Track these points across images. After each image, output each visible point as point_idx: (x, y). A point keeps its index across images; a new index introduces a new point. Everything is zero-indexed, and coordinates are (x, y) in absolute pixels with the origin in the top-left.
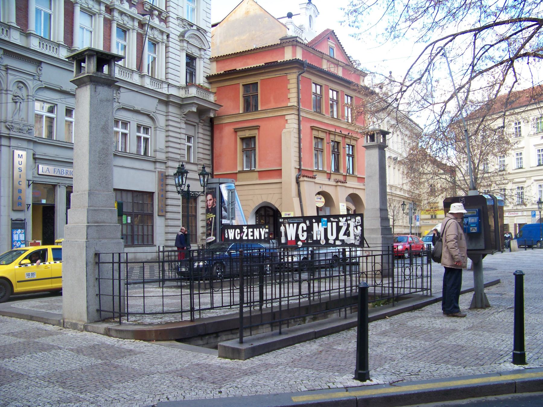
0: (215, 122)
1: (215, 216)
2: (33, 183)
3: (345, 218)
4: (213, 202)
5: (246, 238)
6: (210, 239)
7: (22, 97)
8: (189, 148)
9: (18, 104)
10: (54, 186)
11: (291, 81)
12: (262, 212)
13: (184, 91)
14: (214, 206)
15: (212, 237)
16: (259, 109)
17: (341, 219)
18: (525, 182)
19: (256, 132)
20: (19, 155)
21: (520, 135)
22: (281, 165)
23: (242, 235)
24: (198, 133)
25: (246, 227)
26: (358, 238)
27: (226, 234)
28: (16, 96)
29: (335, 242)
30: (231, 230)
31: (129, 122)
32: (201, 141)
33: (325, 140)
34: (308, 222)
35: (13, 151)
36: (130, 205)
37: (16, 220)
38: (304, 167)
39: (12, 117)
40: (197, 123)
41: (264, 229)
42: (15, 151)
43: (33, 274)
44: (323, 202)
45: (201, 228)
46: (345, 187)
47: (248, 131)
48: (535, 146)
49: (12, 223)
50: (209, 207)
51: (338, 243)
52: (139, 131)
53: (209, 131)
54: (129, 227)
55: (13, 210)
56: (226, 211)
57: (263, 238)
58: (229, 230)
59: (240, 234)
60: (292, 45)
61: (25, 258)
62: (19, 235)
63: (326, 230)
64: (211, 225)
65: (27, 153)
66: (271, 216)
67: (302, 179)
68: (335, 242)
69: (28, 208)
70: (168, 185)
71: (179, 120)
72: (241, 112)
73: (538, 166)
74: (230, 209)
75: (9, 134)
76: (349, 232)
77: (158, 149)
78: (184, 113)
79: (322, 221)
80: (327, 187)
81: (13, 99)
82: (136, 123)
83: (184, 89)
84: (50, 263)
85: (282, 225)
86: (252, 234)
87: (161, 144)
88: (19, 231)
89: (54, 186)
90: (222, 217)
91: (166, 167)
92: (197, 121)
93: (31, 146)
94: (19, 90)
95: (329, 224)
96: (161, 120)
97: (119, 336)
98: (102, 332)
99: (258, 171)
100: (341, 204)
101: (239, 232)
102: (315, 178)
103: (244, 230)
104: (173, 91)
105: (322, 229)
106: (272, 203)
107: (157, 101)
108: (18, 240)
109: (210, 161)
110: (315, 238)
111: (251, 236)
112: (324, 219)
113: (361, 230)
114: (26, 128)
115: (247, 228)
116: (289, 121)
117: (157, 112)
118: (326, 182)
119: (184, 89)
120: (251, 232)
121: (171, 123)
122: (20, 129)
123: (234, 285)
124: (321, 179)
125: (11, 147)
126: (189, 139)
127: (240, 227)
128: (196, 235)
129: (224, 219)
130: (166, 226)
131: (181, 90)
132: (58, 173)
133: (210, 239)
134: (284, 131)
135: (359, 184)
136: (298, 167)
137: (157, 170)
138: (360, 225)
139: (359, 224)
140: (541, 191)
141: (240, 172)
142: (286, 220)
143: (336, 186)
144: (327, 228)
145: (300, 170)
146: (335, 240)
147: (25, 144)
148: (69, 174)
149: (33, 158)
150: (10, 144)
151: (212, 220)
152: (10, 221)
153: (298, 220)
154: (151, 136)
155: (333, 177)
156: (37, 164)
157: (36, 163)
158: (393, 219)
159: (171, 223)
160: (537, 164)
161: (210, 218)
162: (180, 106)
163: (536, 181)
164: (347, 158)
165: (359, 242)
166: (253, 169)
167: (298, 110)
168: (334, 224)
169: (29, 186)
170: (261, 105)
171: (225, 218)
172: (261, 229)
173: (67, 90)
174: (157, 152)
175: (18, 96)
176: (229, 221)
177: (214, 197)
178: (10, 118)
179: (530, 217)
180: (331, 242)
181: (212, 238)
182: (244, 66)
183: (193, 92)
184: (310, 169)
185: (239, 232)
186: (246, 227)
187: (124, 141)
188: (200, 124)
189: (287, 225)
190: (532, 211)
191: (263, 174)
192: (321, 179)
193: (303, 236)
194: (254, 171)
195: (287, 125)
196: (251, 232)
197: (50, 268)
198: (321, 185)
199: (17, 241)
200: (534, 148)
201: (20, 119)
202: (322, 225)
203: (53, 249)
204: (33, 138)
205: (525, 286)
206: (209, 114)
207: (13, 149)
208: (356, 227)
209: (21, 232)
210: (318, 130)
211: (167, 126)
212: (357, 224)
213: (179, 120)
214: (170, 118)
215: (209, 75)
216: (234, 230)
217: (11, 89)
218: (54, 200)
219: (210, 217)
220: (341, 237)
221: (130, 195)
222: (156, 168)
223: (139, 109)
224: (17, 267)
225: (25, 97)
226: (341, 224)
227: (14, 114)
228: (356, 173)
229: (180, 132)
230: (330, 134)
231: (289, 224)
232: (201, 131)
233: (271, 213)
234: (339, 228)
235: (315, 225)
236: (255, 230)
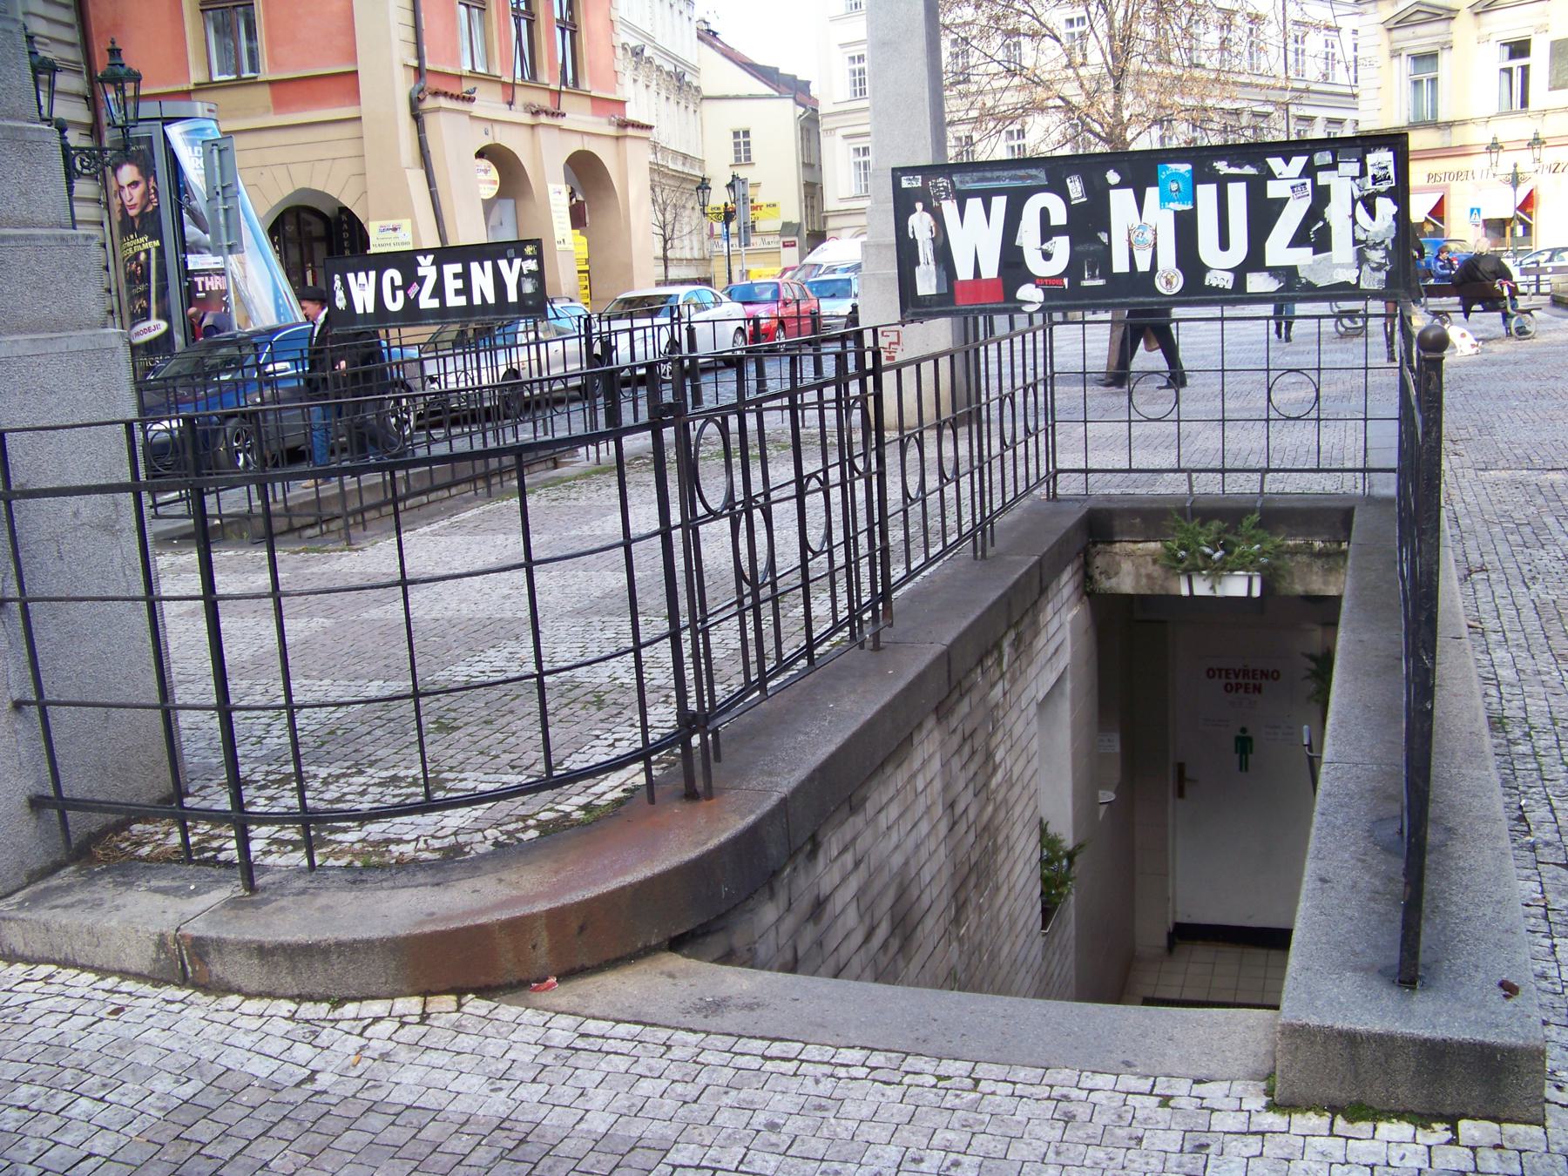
1: (157, 243)
3: (1299, 162)
4: (146, 194)
5: (435, 303)
6: (149, 330)
12: (290, 228)
14: (150, 208)
15: (153, 322)
17: (1275, 163)
22: (353, 56)
23: (412, 293)
25: (430, 258)
26: (1377, 256)
27: (340, 294)
29: (1240, 282)
34: (1075, 188)
38: (430, 62)
41: (517, 262)
44: (495, 182)
46: (560, 129)
48: (842, 46)
50: (132, 213)
51: (1258, 283)
56: (198, 220)
57: (512, 297)
58: (351, 276)
59: (405, 287)
63: (1186, 226)
66: (318, 239)
67: (429, 103)
68: (1240, 282)
76: (1327, 229)
79: (1162, 176)
80: (507, 130)
85: (919, 206)
86: (459, 284)
90: (184, 247)
95: (1207, 193)
97: (289, 983)
98: (139, 957)
99: (271, 83)
100: (551, 187)
101: (399, 282)
102: (471, 100)
103: (421, 272)
105: (1160, 217)
106: (313, 187)
110: (1120, 265)
111: (458, 292)
112: (1173, 167)
113: (1395, 217)
115: (439, 263)
118: (503, 113)
120: (456, 276)
124: (488, 102)
127: (406, 261)
129: (193, 253)
133: (149, 330)
135: (596, 119)
136: (415, 63)
138: (1389, 194)
139: (1384, 187)
141: (201, 88)
142: (943, 182)
143: (533, 127)
144: (1193, 213)
145: (419, 71)
146: (1240, 273)
153: (1011, 179)
155: (522, 96)
158: (664, 236)
161: (137, 255)
163: (846, 137)
164: (558, 32)
165: (1382, 275)
166: (247, 74)
168: (1238, 194)
171: (198, 249)
172: (503, 264)
176: (220, 259)
177: (147, 170)
180: (1219, 278)
181: (156, 327)
184: (450, 70)
185: (398, 282)
186: (430, 258)
189: (949, 208)
191: (287, 90)
192: (488, 102)
193: (1047, 256)
194: (253, 83)
196: (456, 276)
198: (488, 125)
202: (1165, 199)
208: (1369, 203)
212: (1369, 185)
216: (372, 274)
219: (140, 248)
220: (1278, 250)
226: (1274, 190)
228: (586, 85)
231: (961, 199)
233: (317, 228)
234: (1263, 215)
235: (1121, 201)
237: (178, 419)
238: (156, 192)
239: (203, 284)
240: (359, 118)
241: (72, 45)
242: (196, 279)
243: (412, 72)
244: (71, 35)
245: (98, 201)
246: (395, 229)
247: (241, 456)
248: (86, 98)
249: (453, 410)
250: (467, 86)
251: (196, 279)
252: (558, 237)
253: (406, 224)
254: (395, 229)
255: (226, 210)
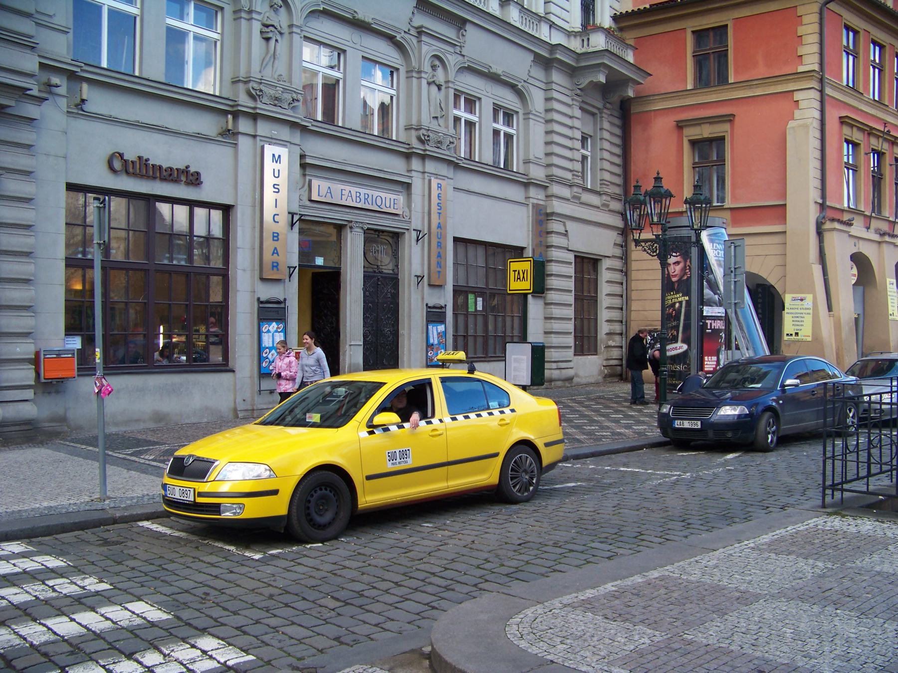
0: (632, 107)
1: (687, 298)
2: (300, 220)
4: (684, 268)
7: (278, 27)
8: (584, 158)
9: (273, 42)
10: (340, 228)
11: (806, 20)
13: (579, 40)
14: (685, 278)
15: (679, 344)
19: (727, 127)
20: (274, 155)
24: (601, 129)
28: (267, 26)
31: (480, 99)
32: (606, 145)
33: (862, 146)
35: (263, 148)
36: (482, 272)
37: (268, 302)
39: (260, 72)
40: (599, 109)
42: (267, 147)
43: (404, 454)
44: (854, 275)
45: (607, 323)
47: (708, 125)
49: (259, 308)
50: (674, 279)
52: (495, 120)
53: (618, 126)
54: (480, 320)
55: (262, 279)
61: (382, 409)
62: (273, 335)
64: (677, 318)
67: (828, 225)
69: (290, 276)
70: (551, 232)
71: (568, 100)
72: (689, 87)
74: (733, 283)
75: (255, 108)
77: (531, 157)
78: (579, 87)
81: (261, 32)
82: (492, 101)
83: (578, 38)
84: (441, 421)
87: (538, 150)
88: (274, 325)
89: (340, 228)
90: (702, 302)
91: (547, 196)
92: (600, 105)
93: (297, 137)
94: (272, 13)
96: (537, 99)
99: (731, 209)
100: (888, 280)
104: (557, 38)
106: (760, 274)
107: (531, 57)
108: (271, 345)
109: (621, 188)
114: (288, 97)
116: (802, 105)
117: (531, 81)
119: (578, 38)
121: (556, 106)
122: (276, 99)
124: (857, 228)
125: (258, 138)
126: (584, 139)
128: (596, 337)
129: (707, 306)
130: (546, 318)
131: (572, 38)
132: (350, 198)
134: (791, 124)
136: (820, 201)
137: (531, 200)
143: (879, 243)
145: (823, 206)
147: (284, 133)
148: (370, 203)
149: (301, 165)
150: (256, 130)
151: (681, 306)
152: (256, 303)
154: (517, 130)
156: (308, 178)
157: (304, 175)
159: (557, 312)
161: (675, 303)
162: (572, 72)
167: (821, 81)
169: (292, 225)
170: (736, 72)
171: (710, 303)
173: (367, 20)
174: (531, 165)
175: (273, 26)
177: (686, 256)
178: (255, 74)
181: (681, 347)
183: (599, 41)
184: (838, 206)
187: (468, 138)
188: (605, 111)
192: (857, 228)
195: (797, 113)
197: (444, 436)
198: (856, 240)
199: (270, 349)
201: (276, 77)
203: (444, 380)
204: (302, 120)
206: (626, 92)
207: (262, 143)
209: (278, 328)
210: (852, 126)
211: (547, 111)
213: (568, 100)
214: (555, 95)
215: (618, 14)
217: (258, 10)
218: (340, 258)
219: (676, 300)
221: (481, 251)
222: (527, 198)
223: (499, 72)
224: (364, 433)
225: (285, 30)
227: (263, 66)
229: (570, 124)
230: (869, 134)
232: (606, 125)
238: (690, 269)
239: (711, 324)
240: (785, 232)
241: (618, 185)
242: (707, 321)
243: (818, 207)
244: (618, 180)
245: (622, 271)
246: (802, 300)
247: (770, 436)
248: (622, 214)
249: (872, 418)
250: (846, 217)
251: (707, 321)
252: (890, 312)
253: (809, 298)
254: (802, 300)
255: (735, 282)
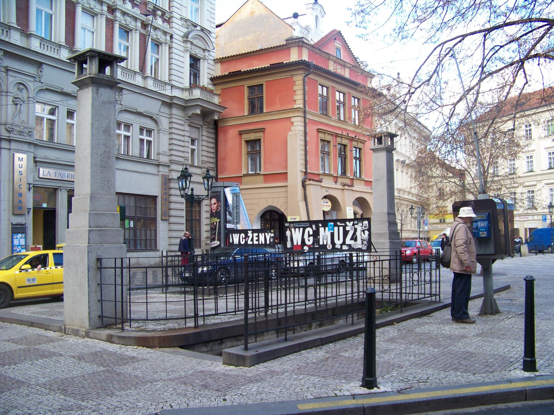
0: (219, 124)
1: (219, 220)
2: (33, 186)
3: (352, 223)
4: (217, 206)
5: (251, 243)
6: (215, 244)
7: (22, 99)
8: (193, 151)
9: (19, 106)
10: (55, 190)
11: (297, 83)
12: (268, 217)
13: (188, 92)
14: (218, 211)
15: (216, 242)
16: (265, 111)
17: (348, 223)
18: (535, 185)
19: (261, 134)
20: (19, 158)
21: (531, 138)
22: (286, 168)
23: (246, 240)
24: (202, 135)
25: (251, 231)
26: (365, 242)
27: (231, 239)
28: (16, 98)
29: (341, 247)
30: (236, 234)
31: (132, 125)
32: (205, 143)
33: (332, 142)
34: (314, 227)
35: (14, 154)
36: (133, 209)
37: (16, 225)
38: (310, 170)
39: (12, 120)
40: (201, 125)
41: (270, 234)
42: (16, 154)
43: (34, 280)
44: (330, 206)
45: (205, 233)
46: (352, 190)
47: (253, 133)
48: (546, 148)
49: (12, 227)
50: (214, 211)
51: (345, 247)
52: (141, 133)
53: (213, 133)
54: (132, 232)
55: (14, 214)
56: (230, 215)
57: (268, 242)
58: (234, 235)
59: (245, 238)
60: (298, 46)
61: (26, 263)
62: (19, 240)
63: (332, 235)
64: (215, 229)
65: (28, 156)
66: (277, 220)
67: (308, 182)
68: (341, 247)
69: (29, 212)
70: (171, 188)
71: (182, 123)
72: (246, 114)
73: (549, 169)
74: (235, 213)
75: (9, 137)
76: (356, 237)
77: (161, 152)
78: (188, 116)
79: (329, 225)
80: (334, 190)
81: (13, 101)
82: (139, 125)
83: (187, 91)
84: (51, 268)
85: (288, 229)
86: (257, 238)
87: (164, 147)
88: (20, 235)
89: (55, 190)
90: (226, 221)
91: (169, 170)
92: (201, 124)
93: (32, 149)
94: (19, 92)
95: (336, 228)
96: (164, 123)
97: (121, 342)
98: (104, 338)
99: (264, 175)
100: (348, 208)
101: (244, 237)
102: (321, 182)
103: (249, 235)
104: (177, 93)
105: (328, 233)
107: (161, 103)
108: (18, 244)
109: (215, 164)
110: (321, 243)
111: (256, 240)
112: (330, 223)
113: (368, 235)
114: (27, 131)
115: (253, 233)
116: (295, 124)
117: (160, 114)
118: (333, 185)
119: (187, 91)
120: (256, 236)
121: (174, 125)
122: (20, 132)
123: (238, 291)
124: (327, 182)
125: (11, 150)
126: (193, 141)
127: (245, 232)
128: (200, 239)
129: (228, 223)
130: (169, 230)
131: (184, 91)
132: (60, 176)
133: (215, 244)
134: (290, 133)
135: (366, 187)
136: (304, 171)
137: (161, 173)
140: (552, 194)
141: (245, 175)
142: (292, 225)
143: (343, 189)
144: (334, 233)
145: (306, 173)
146: (341, 245)
147: (25, 147)
148: (70, 177)
149: (34, 161)
150: (10, 147)
151: (216, 224)
152: (10, 226)
153: (304, 225)
154: (154, 138)
155: (340, 180)
156: (38, 167)
157: (36, 166)
158: (401, 223)
159: (174, 227)
160: (548, 167)
161: (214, 223)
162: (184, 108)
163: (547, 184)
164: (354, 161)
165: (366, 247)
166: (258, 172)
167: (305, 112)
168: (341, 229)
169: (30, 189)
170: (267, 107)
171: (229, 222)
172: (266, 234)
173: (69, 92)
174: (160, 155)
175: (19, 98)
176: (234, 225)
177: (218, 200)
178: (10, 121)
179: (541, 221)
180: (338, 246)
181: (217, 243)
182: (249, 67)
183: (197, 93)
184: (316, 173)
185: (244, 237)
186: (251, 231)
187: (126, 144)
188: (204, 126)
189: (293, 230)
190: (543, 215)
191: (268, 177)
192: (327, 182)
193: (309, 240)
194: (259, 174)
195: (293, 128)
196: (256, 236)
197: (51, 274)
198: (328, 189)
199: (18, 246)
200: (545, 150)
201: (21, 121)
202: (329, 230)
203: (54, 254)
204: (34, 141)
205: (536, 291)
206: (214, 117)
207: (13, 152)
209: (22, 236)
210: (325, 133)
211: (170, 128)
212: (364, 228)
213: (182, 123)
214: (174, 120)
215: (213, 76)
216: (238, 234)
217: (11, 91)
218: (55, 204)
219: (214, 221)
220: (348, 241)
221: (132, 199)
222: (159, 172)
223: (142, 111)
224: (17, 272)
225: (26, 99)
226: (347, 228)
227: (14, 116)
228: (363, 177)
229: (183, 134)
230: (336, 136)
231: (295, 228)
232: (205, 133)
233: (277, 217)
234: (346, 233)
235: (321, 230)
236: (260, 234)
237: (207, 266)
